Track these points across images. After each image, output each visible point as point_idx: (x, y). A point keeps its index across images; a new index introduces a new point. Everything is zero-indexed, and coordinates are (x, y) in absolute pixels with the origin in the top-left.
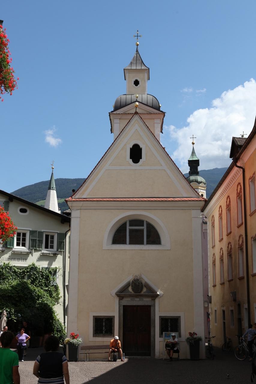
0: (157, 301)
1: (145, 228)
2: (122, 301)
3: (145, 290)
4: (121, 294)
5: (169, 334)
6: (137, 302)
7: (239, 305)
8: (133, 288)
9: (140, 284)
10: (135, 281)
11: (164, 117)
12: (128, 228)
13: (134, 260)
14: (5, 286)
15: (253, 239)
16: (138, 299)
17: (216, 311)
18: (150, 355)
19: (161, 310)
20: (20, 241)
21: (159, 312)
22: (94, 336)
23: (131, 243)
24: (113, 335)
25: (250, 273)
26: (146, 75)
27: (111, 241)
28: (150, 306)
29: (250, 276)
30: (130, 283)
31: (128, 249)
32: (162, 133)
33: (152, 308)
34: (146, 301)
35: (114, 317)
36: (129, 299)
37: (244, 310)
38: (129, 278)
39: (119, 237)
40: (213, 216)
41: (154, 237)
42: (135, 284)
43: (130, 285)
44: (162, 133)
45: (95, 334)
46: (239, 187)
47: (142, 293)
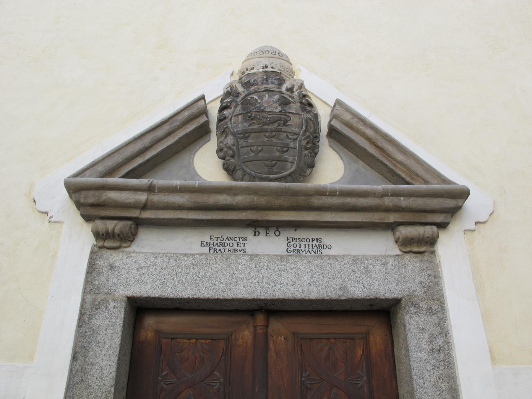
0: (450, 248)
2: (117, 258)
3: (331, 170)
4: (117, 200)
6: (266, 268)
8: (230, 140)
9: (295, 107)
10: (247, 85)
14: (112, 396)
16: (268, 246)
21: (493, 359)
28: (384, 312)
30: (204, 112)
33: (414, 327)
34: (352, 265)
42: (246, 103)
43: (202, 132)
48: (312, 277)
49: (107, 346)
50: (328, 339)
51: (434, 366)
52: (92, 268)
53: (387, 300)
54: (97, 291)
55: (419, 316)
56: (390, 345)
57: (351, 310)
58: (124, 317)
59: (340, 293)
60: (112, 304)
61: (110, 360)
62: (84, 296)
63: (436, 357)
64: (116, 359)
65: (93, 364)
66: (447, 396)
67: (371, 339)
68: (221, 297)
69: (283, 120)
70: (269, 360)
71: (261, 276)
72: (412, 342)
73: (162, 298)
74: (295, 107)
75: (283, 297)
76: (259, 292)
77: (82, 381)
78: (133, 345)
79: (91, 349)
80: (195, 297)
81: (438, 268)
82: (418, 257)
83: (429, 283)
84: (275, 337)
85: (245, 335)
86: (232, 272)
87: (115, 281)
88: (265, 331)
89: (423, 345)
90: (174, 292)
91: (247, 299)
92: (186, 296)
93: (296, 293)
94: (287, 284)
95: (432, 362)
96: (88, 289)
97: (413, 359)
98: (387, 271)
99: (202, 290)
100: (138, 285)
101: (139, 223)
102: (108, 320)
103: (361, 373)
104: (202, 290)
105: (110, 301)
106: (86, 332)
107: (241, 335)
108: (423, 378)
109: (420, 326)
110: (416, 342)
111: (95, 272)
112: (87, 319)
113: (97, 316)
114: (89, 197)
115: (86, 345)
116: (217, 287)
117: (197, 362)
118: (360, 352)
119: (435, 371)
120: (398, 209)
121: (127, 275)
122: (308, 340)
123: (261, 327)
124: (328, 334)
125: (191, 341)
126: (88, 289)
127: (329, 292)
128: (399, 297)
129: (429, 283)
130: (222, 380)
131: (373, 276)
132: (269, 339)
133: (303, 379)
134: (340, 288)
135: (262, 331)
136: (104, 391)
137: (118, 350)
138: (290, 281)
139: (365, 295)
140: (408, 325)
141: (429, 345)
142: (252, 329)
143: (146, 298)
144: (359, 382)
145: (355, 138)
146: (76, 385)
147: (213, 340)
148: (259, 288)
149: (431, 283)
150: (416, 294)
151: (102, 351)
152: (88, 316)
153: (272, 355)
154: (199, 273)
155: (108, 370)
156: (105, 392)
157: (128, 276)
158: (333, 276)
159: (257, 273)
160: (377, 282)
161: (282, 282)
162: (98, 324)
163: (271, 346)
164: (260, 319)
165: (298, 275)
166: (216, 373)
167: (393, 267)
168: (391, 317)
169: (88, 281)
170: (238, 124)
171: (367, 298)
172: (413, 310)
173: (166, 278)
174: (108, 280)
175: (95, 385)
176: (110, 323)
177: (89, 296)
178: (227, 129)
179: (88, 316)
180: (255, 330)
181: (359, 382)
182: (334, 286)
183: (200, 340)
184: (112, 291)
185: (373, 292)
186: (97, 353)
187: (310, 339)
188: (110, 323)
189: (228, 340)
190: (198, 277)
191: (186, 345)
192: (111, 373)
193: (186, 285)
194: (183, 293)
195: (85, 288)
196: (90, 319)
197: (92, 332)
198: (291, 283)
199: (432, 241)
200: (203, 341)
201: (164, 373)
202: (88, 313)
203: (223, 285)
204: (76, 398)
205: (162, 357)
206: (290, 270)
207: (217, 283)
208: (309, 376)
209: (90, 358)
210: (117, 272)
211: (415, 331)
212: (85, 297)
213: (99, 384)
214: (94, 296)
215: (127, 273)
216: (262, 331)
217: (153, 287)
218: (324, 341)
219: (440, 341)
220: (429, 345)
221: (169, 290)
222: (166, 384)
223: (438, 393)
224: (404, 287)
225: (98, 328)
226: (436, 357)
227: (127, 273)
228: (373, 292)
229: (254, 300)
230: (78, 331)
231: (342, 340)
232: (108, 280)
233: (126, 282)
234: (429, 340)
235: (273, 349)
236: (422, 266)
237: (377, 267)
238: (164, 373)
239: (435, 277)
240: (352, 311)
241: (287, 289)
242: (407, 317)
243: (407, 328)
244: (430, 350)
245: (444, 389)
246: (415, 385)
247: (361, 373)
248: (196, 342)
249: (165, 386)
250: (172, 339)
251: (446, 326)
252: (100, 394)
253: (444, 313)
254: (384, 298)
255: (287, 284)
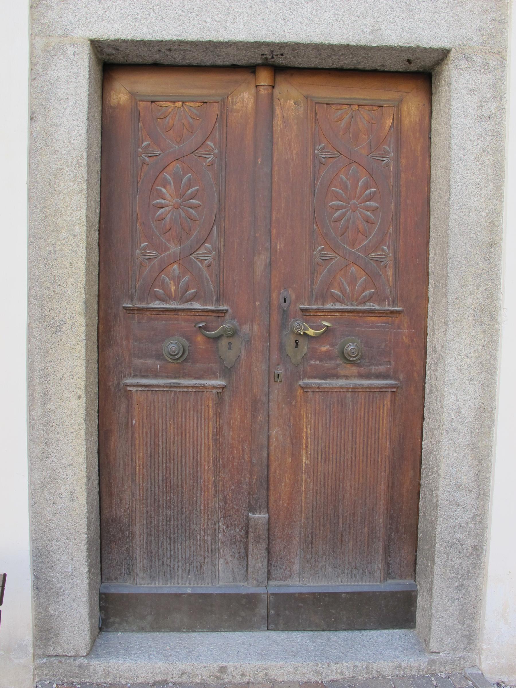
48: (335, 14)
49: (71, 103)
50: (350, 105)
51: (480, 135)
53: (432, 50)
54: (48, 32)
55: (471, 73)
56: (427, 118)
57: (382, 69)
58: (89, 66)
59: (370, 38)
60: (71, 50)
61: (77, 120)
62: (32, 39)
63: (484, 125)
64: (85, 118)
65: (57, 126)
66: (490, 171)
67: (405, 108)
68: (215, 39)
70: (274, 129)
71: (267, 11)
72: (456, 104)
73: (137, 41)
75: (295, 40)
76: (264, 32)
77: (47, 145)
78: (103, 111)
79: (51, 108)
80: (180, 38)
81: (507, 10)
83: (491, 30)
84: (282, 101)
85: (244, 97)
86: (228, 5)
87: (70, 17)
88: (270, 91)
89: (470, 110)
90: (152, 31)
91: (248, 43)
92: (167, 38)
93: (313, 35)
94: (301, 23)
95: (478, 131)
96: (36, 30)
97: (455, 126)
98: (436, 10)
99: (188, 29)
100: (103, 23)
102: (69, 70)
103: (388, 149)
104: (188, 29)
105: (68, 46)
106: (42, 86)
107: (239, 98)
108: (464, 149)
109: (470, 86)
110: (462, 104)
111: (41, 6)
112: (41, 70)
113: (53, 66)
115: (44, 102)
116: (208, 25)
117: (185, 130)
118: (389, 122)
119: (480, 142)
120: (369, 409)
121: (86, 9)
122: (325, 105)
123: (265, 87)
124: (350, 99)
125: (177, 104)
126: (36, 30)
127: (356, 35)
128: (448, 47)
129: (491, 30)
130: (216, 151)
131: (417, 16)
132: (275, 104)
133: (316, 151)
134: (372, 31)
135: (266, 92)
136: (74, 156)
137: (86, 107)
138: (305, 19)
139: (403, 41)
140: (454, 83)
141: (478, 110)
142: (253, 90)
143: (115, 41)
144: (384, 159)
146: (40, 151)
147: (204, 103)
148: (264, 27)
149: (493, 31)
150: (471, 43)
151: (65, 109)
152: (41, 66)
153: (278, 123)
154: (184, 6)
155: (76, 132)
156: (76, 157)
157: (88, 11)
158: (362, 14)
159: (262, 7)
160: (421, 25)
161: (294, 20)
162: (56, 76)
163: (278, 111)
164: (264, 78)
165: (316, 10)
166: (209, 143)
167: (445, 6)
168: (433, 81)
169: (34, 20)
171: (406, 45)
172: (463, 64)
173: (139, 12)
174: (61, 17)
175: (63, 149)
176: (71, 74)
177: (38, 39)
178: (176, 207)
179: (41, 66)
180: (258, 92)
181: (384, 159)
182: (363, 27)
183: (187, 103)
184: (68, 32)
185: (414, 38)
186: (60, 112)
187: (327, 104)
188: (71, 74)
189: (223, 103)
190: (183, 12)
191: (170, 110)
192: (80, 135)
193: (167, 22)
194: (164, 33)
195: (31, 29)
196: (45, 69)
197: (50, 87)
198: (306, 21)
200: (192, 104)
201: (145, 144)
202: (41, 62)
203: (215, 23)
205: (141, 124)
206: (305, 4)
207: (208, 20)
208: (323, 149)
209: (52, 119)
210: (71, 6)
211: (462, 91)
212: (34, 41)
213: (68, 149)
214: (45, 39)
215: (86, 7)
216: (266, 92)
217: (124, 26)
218: (345, 107)
219: (492, 106)
220: (478, 110)
221: (145, 30)
222: (149, 157)
223: (480, 167)
224: (456, 33)
225: (57, 80)
226: (484, 125)
227: (86, 7)
228: (414, 38)
229: (258, 45)
230: (31, 86)
231: (367, 107)
232: (61, 17)
233: (86, 19)
234: (478, 104)
235: (280, 115)
236: (485, 6)
237: (424, 4)
238: (145, 144)
239: (500, 22)
240: (384, 72)
241: (301, 29)
242: (455, 73)
243: (453, 87)
244: (478, 116)
245: (488, 163)
246: (453, 157)
247: (388, 149)
248: (182, 106)
249: (147, 158)
250: (152, 102)
251: (502, 88)
252: (70, 160)
253: (503, 71)
254: (427, 47)
255: (301, 23)
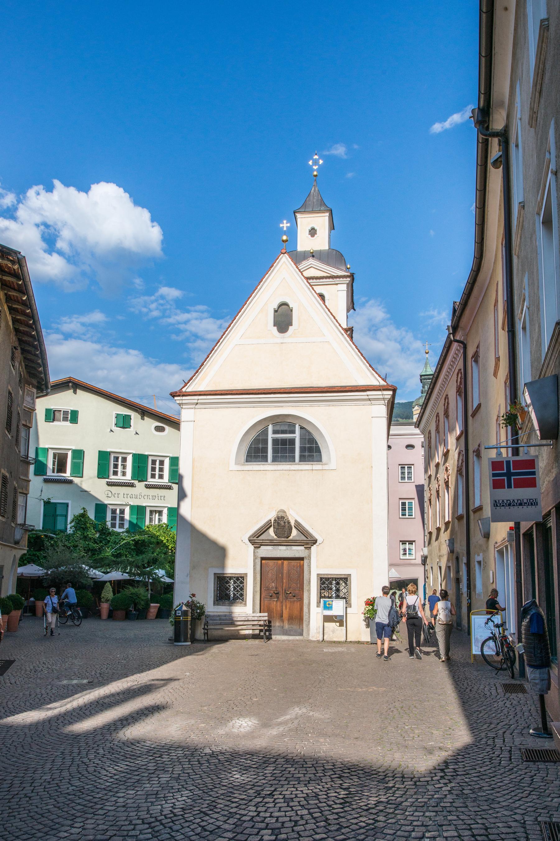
0: (314, 548)
1: (297, 436)
2: (258, 550)
3: (294, 532)
4: (256, 540)
5: (330, 602)
6: (282, 551)
7: (457, 558)
9: (286, 524)
11: (353, 282)
12: (271, 436)
13: (282, 488)
15: (475, 454)
17: (432, 567)
18: (301, 634)
19: (320, 564)
20: (405, 510)
22: (214, 604)
23: (275, 460)
24: (244, 603)
25: (471, 508)
26: (327, 219)
27: (243, 457)
28: (302, 559)
29: (471, 513)
31: (270, 472)
32: (355, 310)
33: (306, 561)
34: (297, 551)
35: (246, 574)
36: (270, 548)
37: (464, 565)
38: (272, 516)
39: (256, 451)
40: (430, 431)
41: (312, 451)
42: (278, 523)
43: (271, 526)
44: (355, 310)
45: (217, 601)
46: (460, 375)
47: (291, 538)
52: (254, 552)
69: (284, 526)
74: (286, 524)
82: (90, 693)
101: (261, 545)
114: (251, 541)
145: (298, 526)
170: (276, 526)
171: (89, 691)
199: (310, 548)
204: (559, 818)
